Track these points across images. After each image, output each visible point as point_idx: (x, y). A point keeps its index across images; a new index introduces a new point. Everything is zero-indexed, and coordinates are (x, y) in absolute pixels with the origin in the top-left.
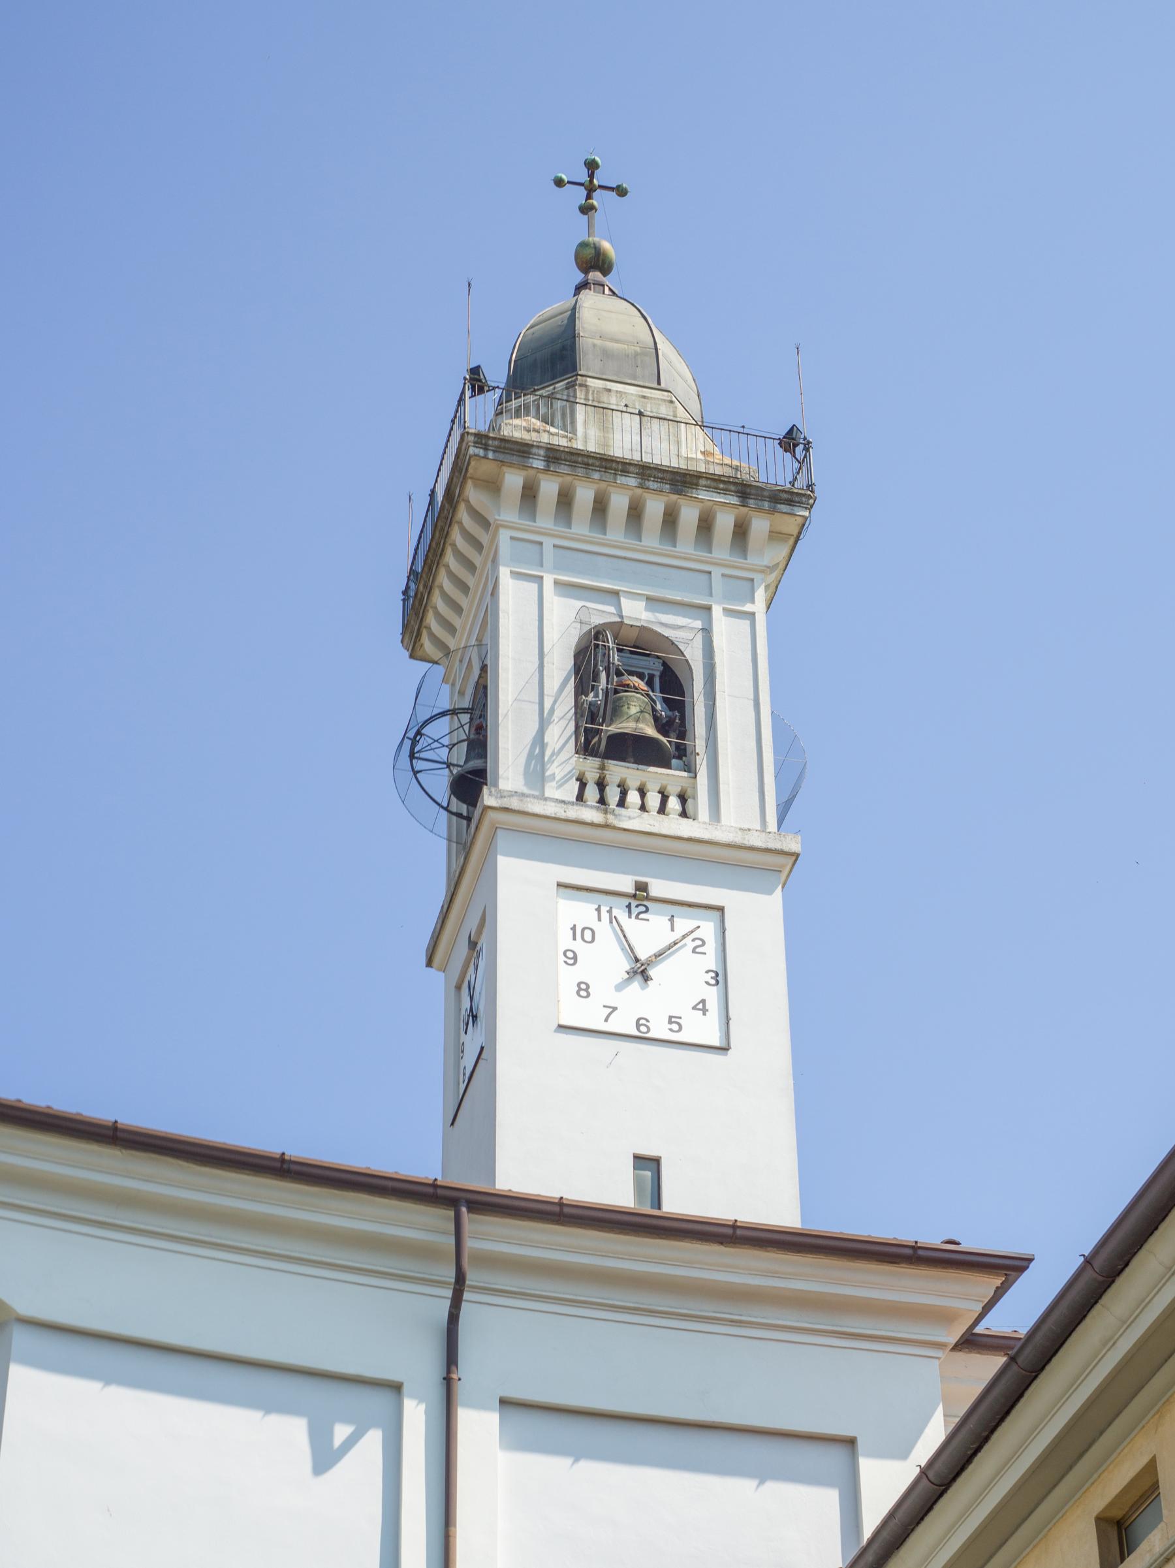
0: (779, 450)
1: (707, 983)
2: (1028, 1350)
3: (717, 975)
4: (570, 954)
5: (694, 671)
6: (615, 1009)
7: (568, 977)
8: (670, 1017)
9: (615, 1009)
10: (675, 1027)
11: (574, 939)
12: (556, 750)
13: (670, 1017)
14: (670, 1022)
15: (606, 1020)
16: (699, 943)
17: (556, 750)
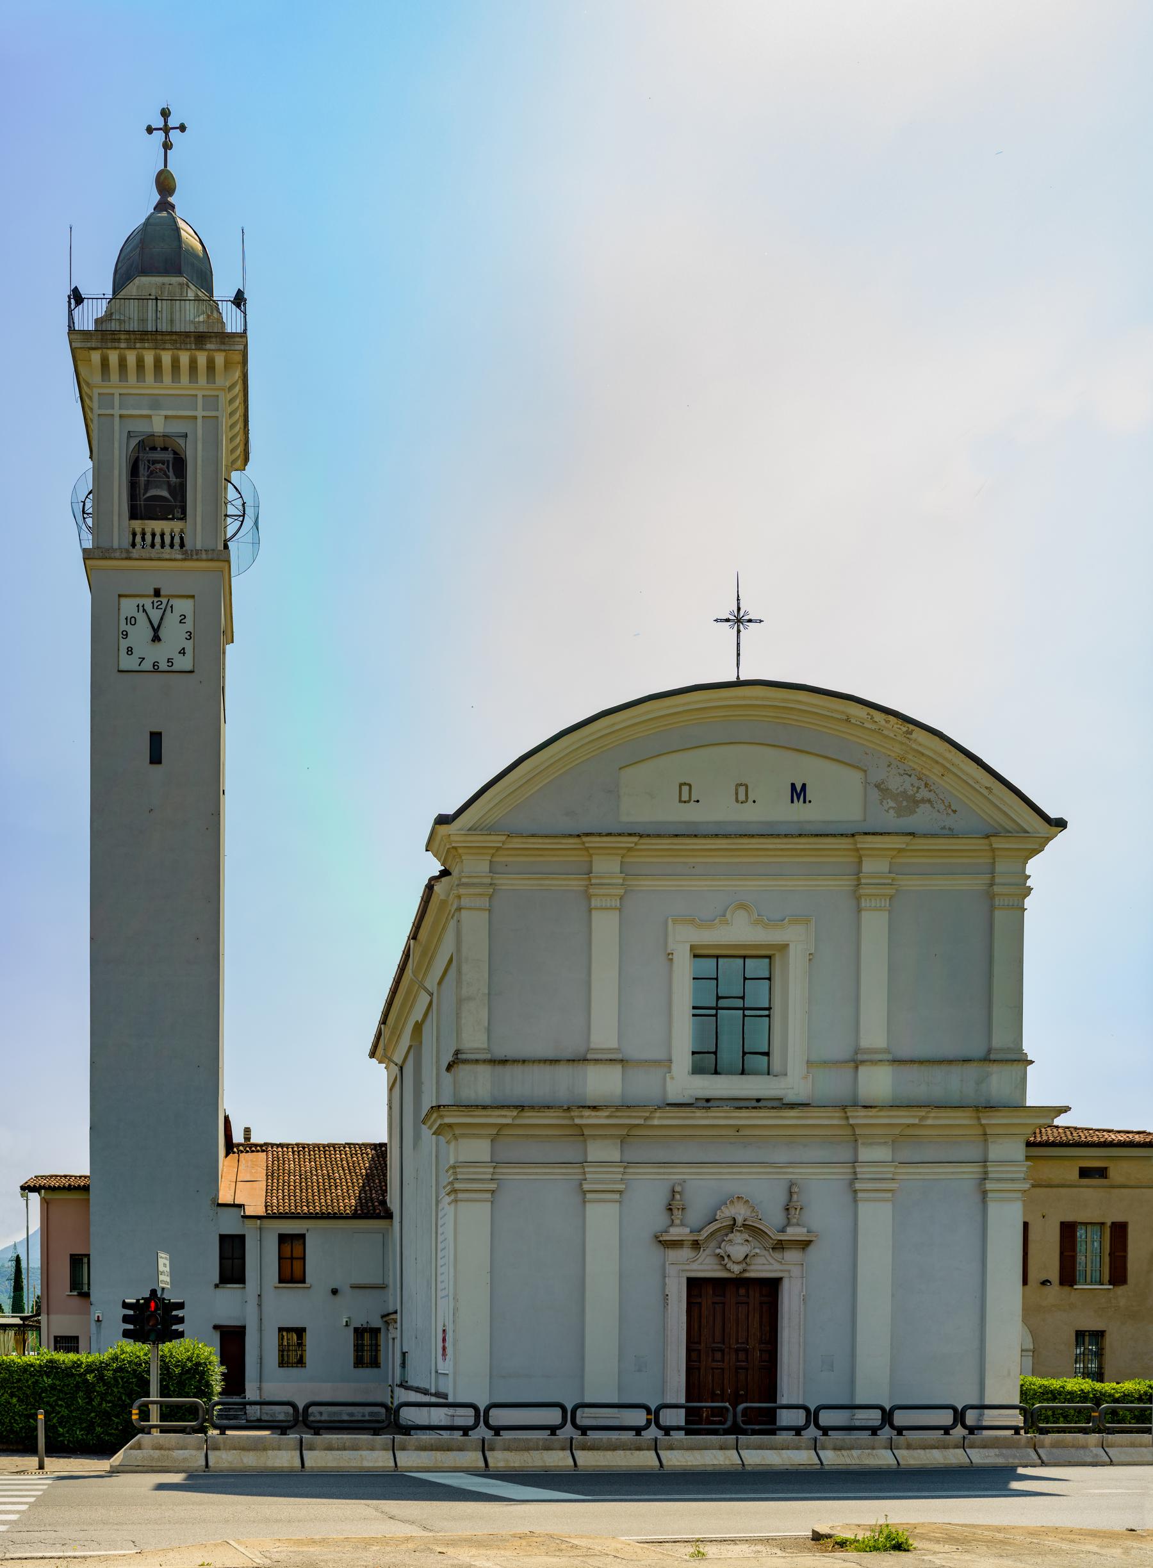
0: (234, 307)
1: (186, 638)
2: (416, 923)
3: (191, 633)
4: (125, 633)
5: (176, 180)
6: (144, 659)
7: (124, 644)
8: (169, 659)
9: (144, 659)
10: (170, 664)
11: (127, 624)
12: (1061, 1121)
13: (169, 659)
14: (168, 662)
15: (140, 665)
16: (183, 617)
17: (1061, 1121)
